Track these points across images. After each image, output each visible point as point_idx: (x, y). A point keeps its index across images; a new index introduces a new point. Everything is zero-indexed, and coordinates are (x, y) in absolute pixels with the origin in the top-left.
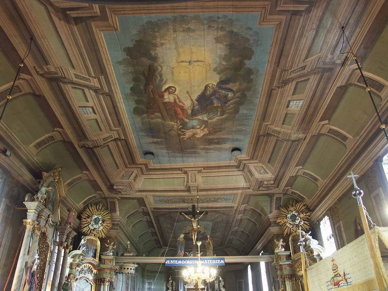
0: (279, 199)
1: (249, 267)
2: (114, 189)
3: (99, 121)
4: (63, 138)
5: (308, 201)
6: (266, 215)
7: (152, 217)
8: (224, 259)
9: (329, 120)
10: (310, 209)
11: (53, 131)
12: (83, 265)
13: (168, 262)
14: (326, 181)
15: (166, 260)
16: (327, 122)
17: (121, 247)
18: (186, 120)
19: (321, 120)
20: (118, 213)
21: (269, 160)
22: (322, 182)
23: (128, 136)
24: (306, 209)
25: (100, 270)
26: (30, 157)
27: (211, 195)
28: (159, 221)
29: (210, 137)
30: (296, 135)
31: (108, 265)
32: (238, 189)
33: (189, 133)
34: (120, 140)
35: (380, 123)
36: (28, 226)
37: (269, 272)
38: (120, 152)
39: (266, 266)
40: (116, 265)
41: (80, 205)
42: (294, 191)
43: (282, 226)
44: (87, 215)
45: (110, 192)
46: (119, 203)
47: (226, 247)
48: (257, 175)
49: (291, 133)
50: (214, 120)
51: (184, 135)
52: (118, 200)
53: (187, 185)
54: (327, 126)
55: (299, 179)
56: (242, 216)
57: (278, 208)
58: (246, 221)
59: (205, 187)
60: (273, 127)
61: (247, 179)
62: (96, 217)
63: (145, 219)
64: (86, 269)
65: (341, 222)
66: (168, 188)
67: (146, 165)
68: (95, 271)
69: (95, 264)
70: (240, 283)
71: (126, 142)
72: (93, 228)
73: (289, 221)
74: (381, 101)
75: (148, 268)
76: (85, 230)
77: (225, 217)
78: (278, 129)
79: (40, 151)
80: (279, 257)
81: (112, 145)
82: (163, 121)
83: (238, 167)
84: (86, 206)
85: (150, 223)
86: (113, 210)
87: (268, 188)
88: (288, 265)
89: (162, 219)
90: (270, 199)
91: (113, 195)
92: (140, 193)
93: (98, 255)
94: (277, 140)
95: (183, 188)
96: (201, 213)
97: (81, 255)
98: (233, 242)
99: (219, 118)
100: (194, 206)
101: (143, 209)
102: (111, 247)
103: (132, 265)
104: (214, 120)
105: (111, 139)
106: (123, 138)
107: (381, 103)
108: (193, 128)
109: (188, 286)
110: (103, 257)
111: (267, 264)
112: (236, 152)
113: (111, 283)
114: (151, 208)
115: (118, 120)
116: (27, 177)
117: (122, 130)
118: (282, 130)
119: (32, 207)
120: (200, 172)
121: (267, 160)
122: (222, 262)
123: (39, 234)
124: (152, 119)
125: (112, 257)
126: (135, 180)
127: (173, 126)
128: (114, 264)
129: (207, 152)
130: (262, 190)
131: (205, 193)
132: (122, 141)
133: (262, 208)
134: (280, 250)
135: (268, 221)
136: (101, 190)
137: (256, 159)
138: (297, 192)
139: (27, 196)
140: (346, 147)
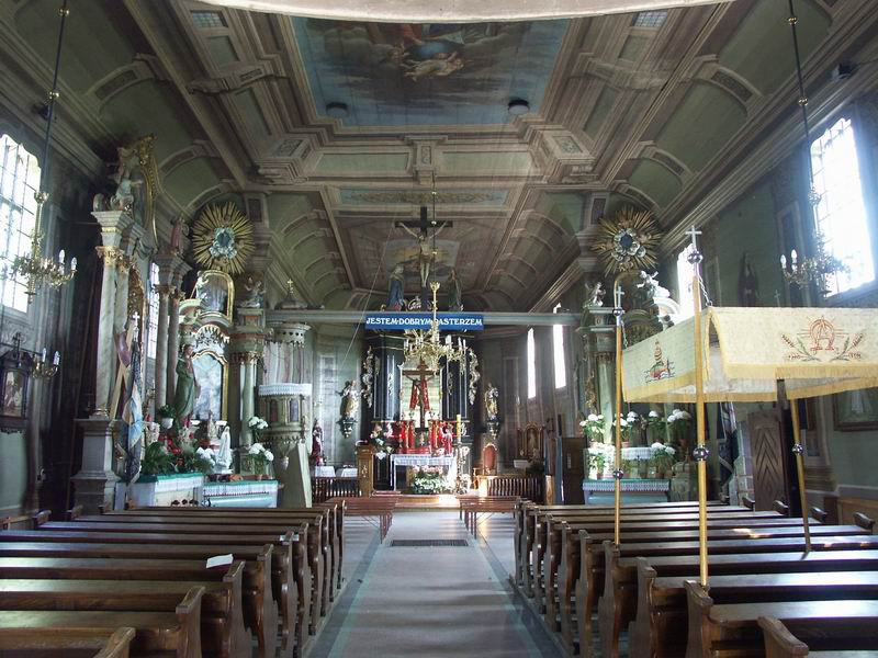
0: (600, 202)
1: (531, 333)
2: (258, 174)
3: (234, 40)
4: (156, 76)
5: (660, 211)
6: (571, 232)
7: (336, 230)
8: (481, 317)
9: (718, 54)
10: (662, 227)
11: (134, 60)
12: (203, 328)
13: (370, 321)
14: (698, 174)
15: (368, 316)
16: (712, 57)
17: (274, 292)
18: (419, 42)
19: (701, 53)
20: (267, 222)
21: (586, 125)
22: (689, 177)
23: (295, 71)
24: (654, 225)
25: (235, 336)
26: (88, 117)
27: (461, 189)
28: (349, 235)
29: (466, 76)
30: (645, 80)
31: (254, 326)
32: (517, 178)
33: (422, 68)
34: (277, 78)
35: (798, 92)
36: (107, 260)
37: (570, 345)
38: (276, 102)
39: (564, 332)
40: (267, 326)
41: (189, 208)
42: (633, 188)
43: (602, 258)
44: (203, 229)
45: (250, 180)
46: (268, 203)
47: (486, 291)
48: (558, 153)
49: (636, 74)
50: (478, 43)
51: (413, 70)
52: (267, 196)
53: (412, 167)
54: (712, 66)
55: (644, 165)
56: (522, 232)
57: (597, 221)
58: (530, 243)
59: (449, 173)
60: (599, 62)
61: (538, 160)
62: (223, 231)
63: (320, 233)
64: (208, 335)
65: (717, 259)
66: (372, 173)
67: (329, 129)
68: (226, 338)
69: (227, 325)
70: (511, 363)
71: (290, 83)
72: (217, 255)
73: (618, 248)
74: (830, 26)
75: (323, 331)
76: (201, 258)
77: (486, 232)
78: (611, 66)
79: (107, 103)
80: (590, 319)
81: (260, 89)
82: (370, 43)
83: (520, 136)
84: (201, 210)
85: (331, 243)
86: (255, 217)
87: (579, 179)
88: (606, 333)
89: (356, 233)
90: (581, 202)
91: (257, 187)
92: (314, 183)
93: (230, 307)
94: (605, 87)
95: (403, 173)
96: (440, 223)
97: (198, 308)
98: (501, 282)
99: (486, 39)
100: (424, 211)
101: (317, 213)
102: (256, 292)
103: (299, 326)
104: (478, 43)
105: (257, 77)
106: (284, 75)
107: (828, 30)
108: (432, 57)
109: (406, 366)
110: (240, 312)
111: (568, 332)
112: (517, 109)
113: (260, 362)
114: (334, 212)
115: (275, 40)
116: (90, 161)
117: (283, 59)
118: (618, 68)
119: (109, 223)
120: (440, 143)
121: (581, 125)
122: (479, 322)
123: (127, 273)
124: (346, 37)
125: (259, 312)
126: (304, 156)
127: (390, 54)
128: (264, 325)
129: (458, 106)
130: (566, 183)
131: (448, 184)
132: (281, 80)
133: (565, 219)
134: (596, 306)
135: (574, 247)
136: (206, 137)
137: (559, 123)
138: (641, 192)
139: (96, 198)
140: (746, 112)
